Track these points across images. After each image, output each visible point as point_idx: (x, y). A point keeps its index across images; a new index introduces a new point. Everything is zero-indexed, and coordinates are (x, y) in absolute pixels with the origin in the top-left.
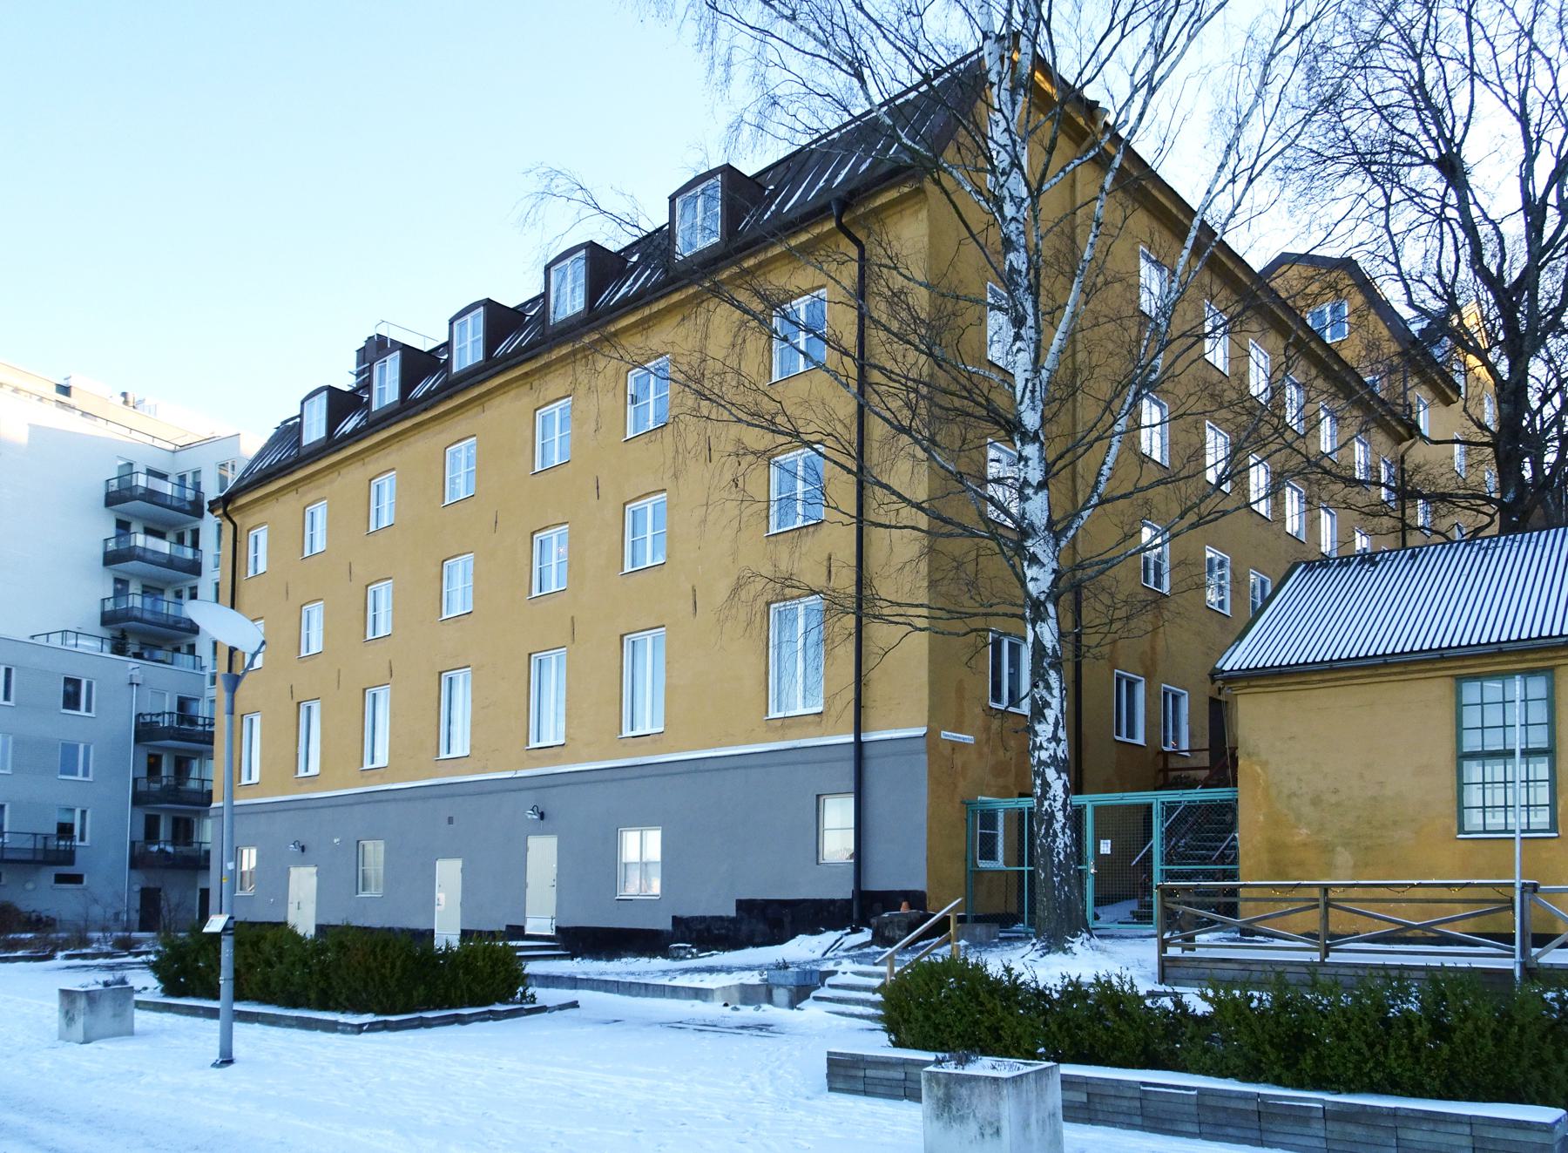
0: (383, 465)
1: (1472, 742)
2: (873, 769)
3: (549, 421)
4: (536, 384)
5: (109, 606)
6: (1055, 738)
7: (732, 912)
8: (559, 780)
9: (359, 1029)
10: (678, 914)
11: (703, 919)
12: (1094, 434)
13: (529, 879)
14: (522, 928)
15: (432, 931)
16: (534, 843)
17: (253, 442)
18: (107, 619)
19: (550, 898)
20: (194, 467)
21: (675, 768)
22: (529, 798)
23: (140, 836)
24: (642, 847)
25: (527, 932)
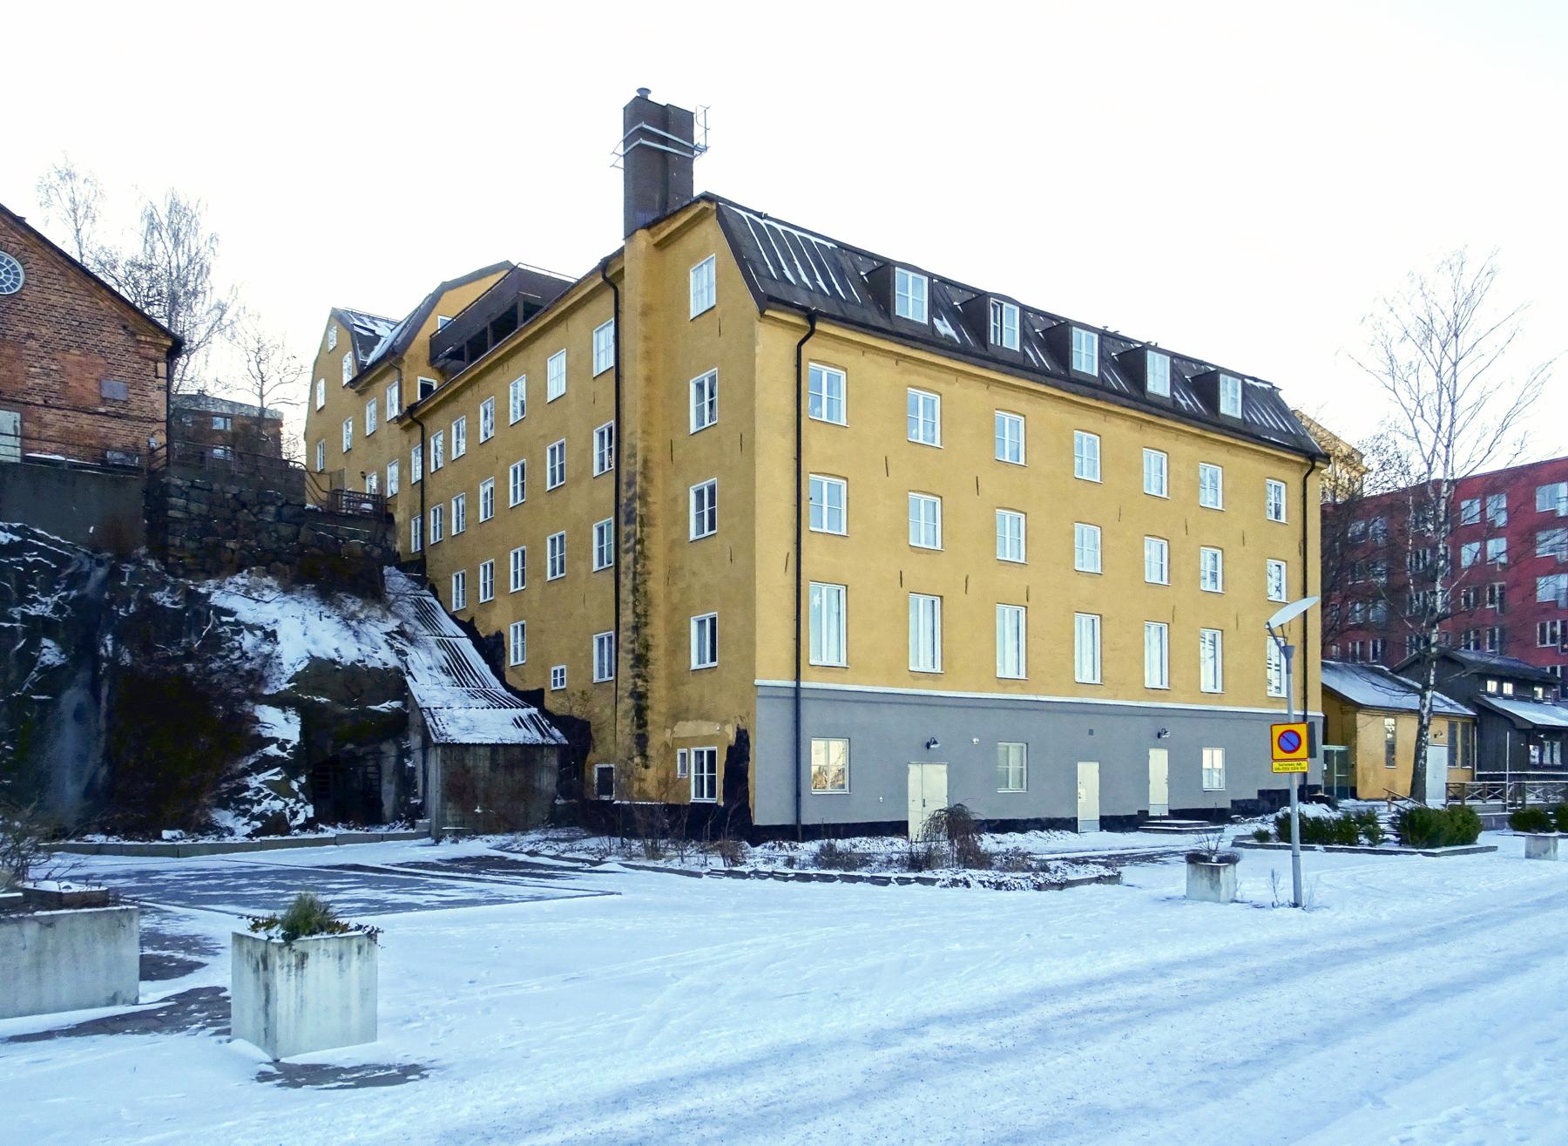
0: (1011, 404)
7: (1255, 797)
15: (906, 823)
21: (1050, 707)
24: (1213, 759)
25: (759, 819)
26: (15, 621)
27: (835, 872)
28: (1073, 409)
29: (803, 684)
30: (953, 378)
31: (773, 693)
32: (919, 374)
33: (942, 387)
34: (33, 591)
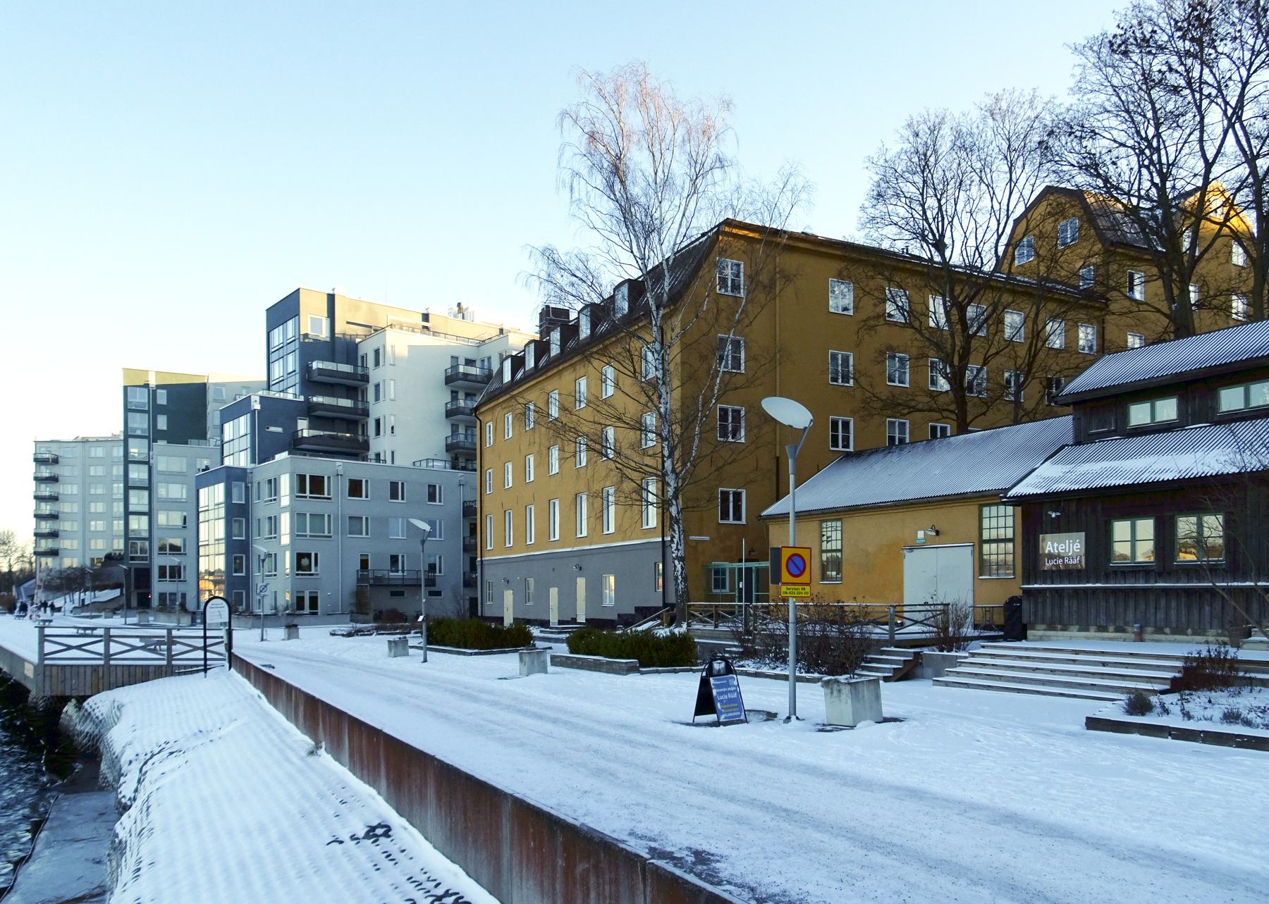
1: (986, 536)
5: (449, 441)
6: (677, 549)
9: (471, 654)
16: (579, 580)
17: (524, 329)
18: (449, 448)
19: (511, 610)
20: (487, 355)
22: (576, 560)
23: (468, 569)
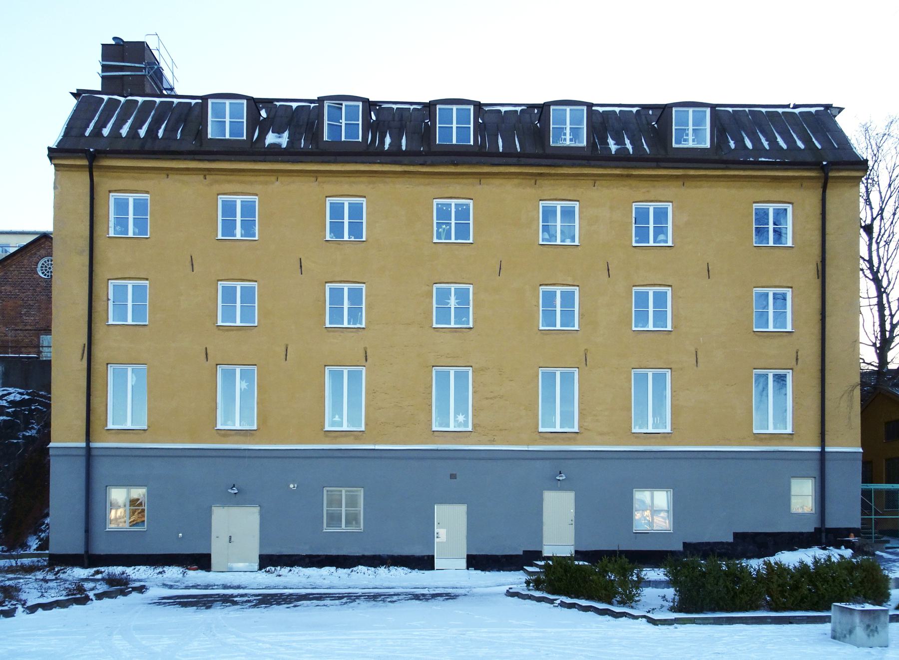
2: (829, 465)
3: (668, 209)
4: (597, 183)
7: (730, 539)
8: (109, 452)
10: (688, 541)
11: (708, 544)
12: (888, 327)
13: (544, 520)
14: (541, 552)
26: (19, 439)
27: (807, 556)
28: (436, 180)
29: (827, 449)
30: (273, 179)
31: (67, 453)
32: (229, 182)
33: (258, 188)
34: (33, 423)
